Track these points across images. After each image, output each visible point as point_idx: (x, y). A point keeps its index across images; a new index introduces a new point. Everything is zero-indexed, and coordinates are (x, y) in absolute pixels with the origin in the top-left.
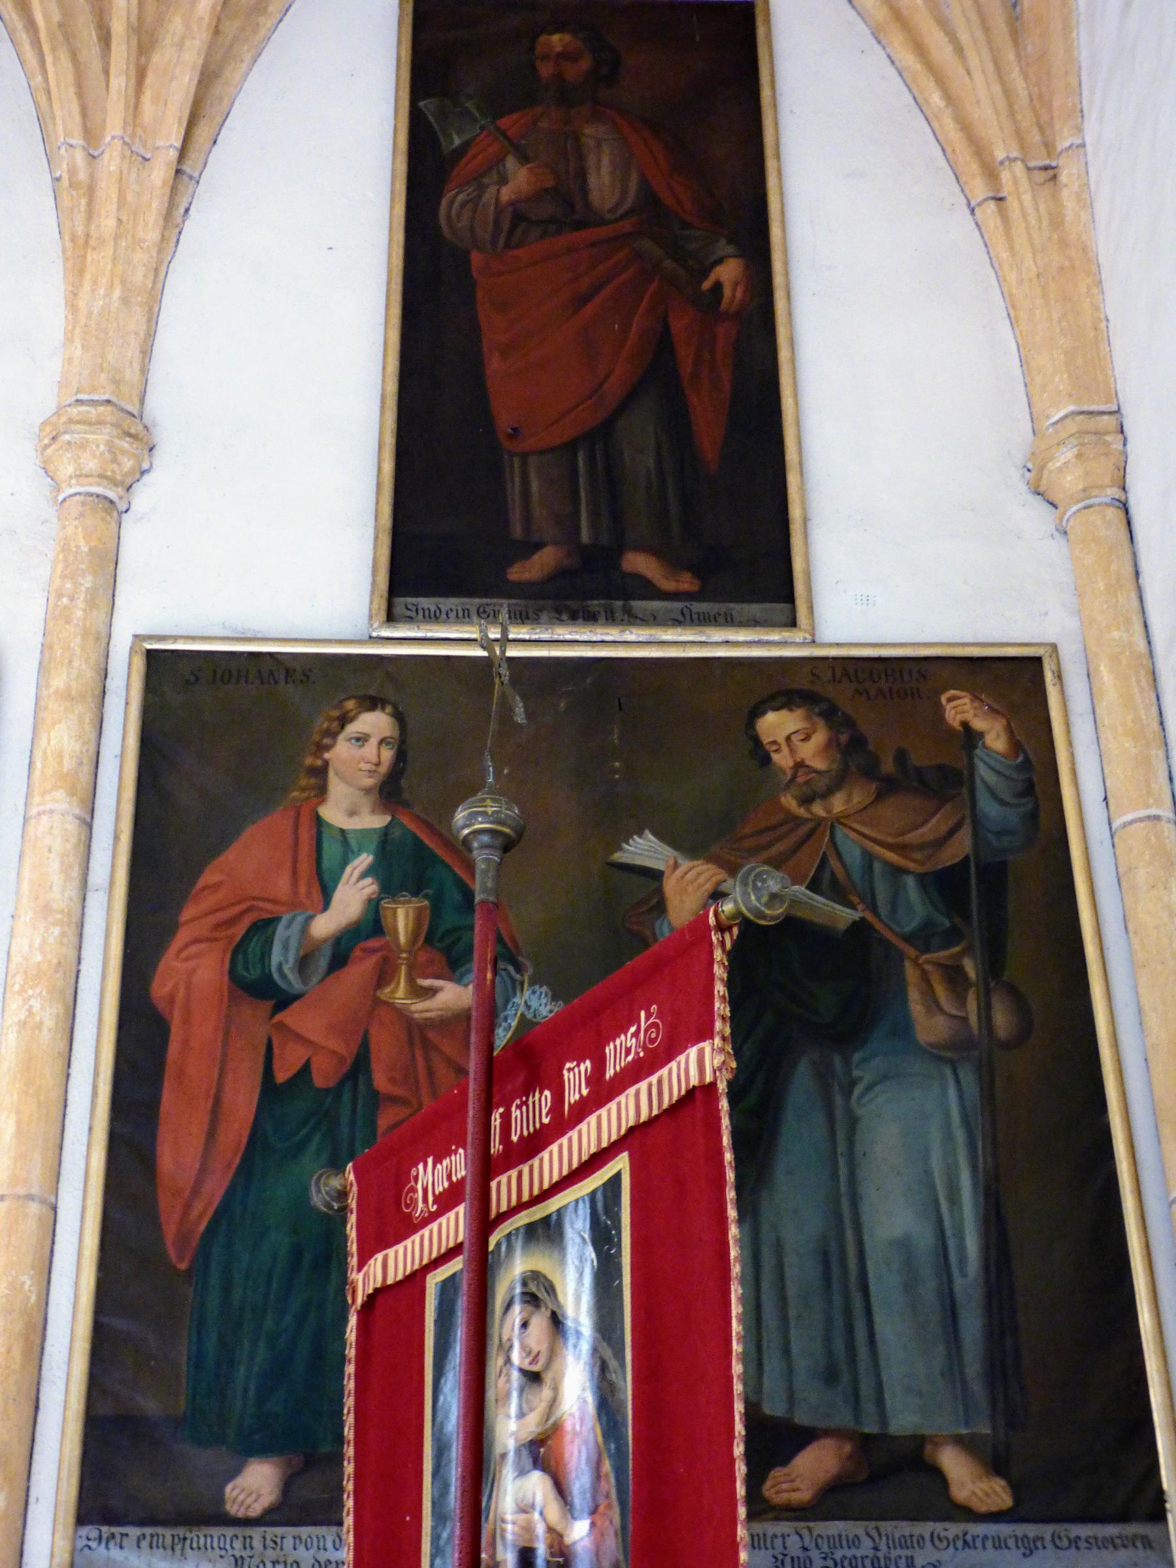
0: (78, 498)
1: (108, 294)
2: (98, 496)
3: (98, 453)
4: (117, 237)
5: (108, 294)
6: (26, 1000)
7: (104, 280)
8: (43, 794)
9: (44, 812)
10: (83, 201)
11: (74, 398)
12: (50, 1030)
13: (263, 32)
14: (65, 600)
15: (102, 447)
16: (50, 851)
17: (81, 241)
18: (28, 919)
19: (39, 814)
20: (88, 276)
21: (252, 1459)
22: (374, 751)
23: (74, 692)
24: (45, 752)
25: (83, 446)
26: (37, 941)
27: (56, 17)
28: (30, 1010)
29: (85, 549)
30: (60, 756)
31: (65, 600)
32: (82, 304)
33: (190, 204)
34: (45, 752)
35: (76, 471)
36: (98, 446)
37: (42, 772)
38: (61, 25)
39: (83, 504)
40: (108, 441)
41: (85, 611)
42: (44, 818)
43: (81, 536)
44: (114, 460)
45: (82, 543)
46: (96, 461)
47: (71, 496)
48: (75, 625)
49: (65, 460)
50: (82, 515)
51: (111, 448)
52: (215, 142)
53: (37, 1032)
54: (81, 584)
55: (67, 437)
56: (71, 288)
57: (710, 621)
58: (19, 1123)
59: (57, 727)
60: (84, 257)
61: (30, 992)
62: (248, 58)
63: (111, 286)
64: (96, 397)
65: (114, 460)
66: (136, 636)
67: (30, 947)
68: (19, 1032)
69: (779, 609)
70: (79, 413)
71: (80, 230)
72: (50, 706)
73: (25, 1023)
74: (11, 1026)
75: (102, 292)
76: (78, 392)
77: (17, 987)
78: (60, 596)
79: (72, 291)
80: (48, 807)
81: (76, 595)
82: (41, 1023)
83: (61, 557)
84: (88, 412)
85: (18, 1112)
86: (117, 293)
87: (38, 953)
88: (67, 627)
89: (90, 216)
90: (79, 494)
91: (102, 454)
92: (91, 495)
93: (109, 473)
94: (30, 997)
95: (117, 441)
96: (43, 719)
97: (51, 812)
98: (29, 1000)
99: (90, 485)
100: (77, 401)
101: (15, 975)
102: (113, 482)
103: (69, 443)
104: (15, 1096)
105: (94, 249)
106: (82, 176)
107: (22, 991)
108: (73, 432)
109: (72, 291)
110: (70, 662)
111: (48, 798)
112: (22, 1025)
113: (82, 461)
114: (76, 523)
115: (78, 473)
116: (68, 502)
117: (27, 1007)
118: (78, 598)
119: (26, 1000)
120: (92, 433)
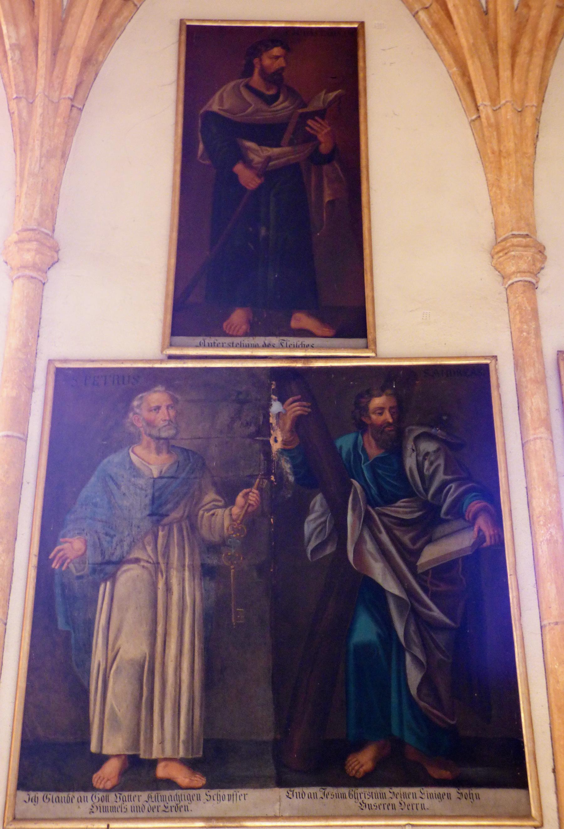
0: (520, 283)
1: (517, 181)
2: (529, 282)
3: (527, 261)
4: (516, 151)
5: (517, 181)
6: (548, 530)
7: (513, 174)
8: (535, 429)
9: (537, 438)
10: (495, 133)
11: (510, 233)
12: (561, 543)
13: (557, 44)
14: (525, 334)
15: (530, 258)
16: (544, 457)
17: (497, 153)
18: (540, 490)
19: (535, 439)
20: (505, 172)
21: (199, 773)
22: (165, 411)
23: (539, 380)
24: (531, 409)
25: (521, 257)
26: (548, 501)
27: (471, 41)
28: (551, 533)
29: (529, 308)
30: (539, 410)
31: (525, 334)
32: (504, 185)
33: (538, 133)
34: (531, 409)
35: (517, 270)
36: (528, 258)
37: (532, 418)
38: (474, 44)
39: (524, 286)
40: (532, 255)
41: (535, 339)
42: (538, 441)
43: (526, 302)
44: (534, 265)
45: (527, 305)
46: (526, 264)
47: (516, 282)
48: (532, 346)
49: (510, 264)
50: (524, 292)
51: (533, 257)
52: (543, 101)
53: (556, 544)
54: (531, 326)
55: (513, 253)
56: (496, 177)
57: (212, 346)
58: (557, 588)
59: (535, 396)
60: (500, 161)
61: (549, 525)
62: (552, 57)
63: (517, 176)
64: (521, 233)
65: (534, 265)
66: (558, 351)
67: (545, 503)
68: (548, 544)
69: (361, 341)
70: (518, 241)
71: (496, 148)
72: (529, 386)
73: (550, 540)
74: (543, 541)
75: (513, 179)
76: (512, 231)
77: (542, 523)
78: (522, 332)
79: (497, 179)
80: (539, 436)
81: (530, 331)
82: (557, 540)
83: (517, 312)
84: (522, 241)
85: (556, 583)
86: (520, 181)
87: (549, 506)
88: (529, 347)
89: (499, 141)
90: (521, 281)
91: (529, 261)
92: (526, 281)
93: (531, 270)
94: (550, 528)
95: (536, 255)
96: (526, 392)
97: (541, 438)
98: (550, 529)
99: (526, 276)
100: (513, 235)
101: (539, 517)
102: (39, 270)
103: (514, 256)
104: (553, 576)
105: (505, 158)
106: (492, 120)
107: (545, 525)
108: (517, 251)
109: (497, 179)
110: (534, 364)
111: (537, 431)
112: (549, 541)
113: (520, 264)
114: (522, 295)
115: (518, 270)
116: (515, 285)
117: (549, 532)
118: (531, 333)
119: (548, 530)
120: (526, 251)
